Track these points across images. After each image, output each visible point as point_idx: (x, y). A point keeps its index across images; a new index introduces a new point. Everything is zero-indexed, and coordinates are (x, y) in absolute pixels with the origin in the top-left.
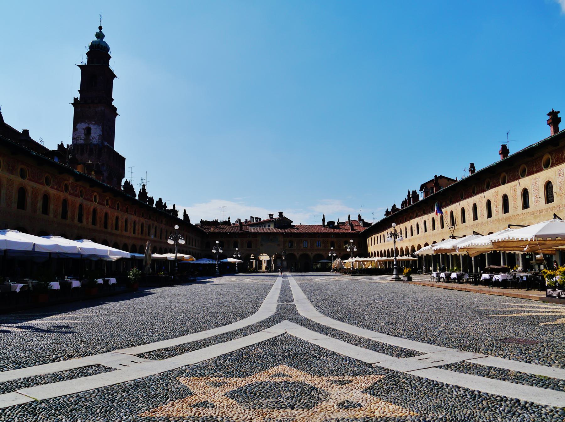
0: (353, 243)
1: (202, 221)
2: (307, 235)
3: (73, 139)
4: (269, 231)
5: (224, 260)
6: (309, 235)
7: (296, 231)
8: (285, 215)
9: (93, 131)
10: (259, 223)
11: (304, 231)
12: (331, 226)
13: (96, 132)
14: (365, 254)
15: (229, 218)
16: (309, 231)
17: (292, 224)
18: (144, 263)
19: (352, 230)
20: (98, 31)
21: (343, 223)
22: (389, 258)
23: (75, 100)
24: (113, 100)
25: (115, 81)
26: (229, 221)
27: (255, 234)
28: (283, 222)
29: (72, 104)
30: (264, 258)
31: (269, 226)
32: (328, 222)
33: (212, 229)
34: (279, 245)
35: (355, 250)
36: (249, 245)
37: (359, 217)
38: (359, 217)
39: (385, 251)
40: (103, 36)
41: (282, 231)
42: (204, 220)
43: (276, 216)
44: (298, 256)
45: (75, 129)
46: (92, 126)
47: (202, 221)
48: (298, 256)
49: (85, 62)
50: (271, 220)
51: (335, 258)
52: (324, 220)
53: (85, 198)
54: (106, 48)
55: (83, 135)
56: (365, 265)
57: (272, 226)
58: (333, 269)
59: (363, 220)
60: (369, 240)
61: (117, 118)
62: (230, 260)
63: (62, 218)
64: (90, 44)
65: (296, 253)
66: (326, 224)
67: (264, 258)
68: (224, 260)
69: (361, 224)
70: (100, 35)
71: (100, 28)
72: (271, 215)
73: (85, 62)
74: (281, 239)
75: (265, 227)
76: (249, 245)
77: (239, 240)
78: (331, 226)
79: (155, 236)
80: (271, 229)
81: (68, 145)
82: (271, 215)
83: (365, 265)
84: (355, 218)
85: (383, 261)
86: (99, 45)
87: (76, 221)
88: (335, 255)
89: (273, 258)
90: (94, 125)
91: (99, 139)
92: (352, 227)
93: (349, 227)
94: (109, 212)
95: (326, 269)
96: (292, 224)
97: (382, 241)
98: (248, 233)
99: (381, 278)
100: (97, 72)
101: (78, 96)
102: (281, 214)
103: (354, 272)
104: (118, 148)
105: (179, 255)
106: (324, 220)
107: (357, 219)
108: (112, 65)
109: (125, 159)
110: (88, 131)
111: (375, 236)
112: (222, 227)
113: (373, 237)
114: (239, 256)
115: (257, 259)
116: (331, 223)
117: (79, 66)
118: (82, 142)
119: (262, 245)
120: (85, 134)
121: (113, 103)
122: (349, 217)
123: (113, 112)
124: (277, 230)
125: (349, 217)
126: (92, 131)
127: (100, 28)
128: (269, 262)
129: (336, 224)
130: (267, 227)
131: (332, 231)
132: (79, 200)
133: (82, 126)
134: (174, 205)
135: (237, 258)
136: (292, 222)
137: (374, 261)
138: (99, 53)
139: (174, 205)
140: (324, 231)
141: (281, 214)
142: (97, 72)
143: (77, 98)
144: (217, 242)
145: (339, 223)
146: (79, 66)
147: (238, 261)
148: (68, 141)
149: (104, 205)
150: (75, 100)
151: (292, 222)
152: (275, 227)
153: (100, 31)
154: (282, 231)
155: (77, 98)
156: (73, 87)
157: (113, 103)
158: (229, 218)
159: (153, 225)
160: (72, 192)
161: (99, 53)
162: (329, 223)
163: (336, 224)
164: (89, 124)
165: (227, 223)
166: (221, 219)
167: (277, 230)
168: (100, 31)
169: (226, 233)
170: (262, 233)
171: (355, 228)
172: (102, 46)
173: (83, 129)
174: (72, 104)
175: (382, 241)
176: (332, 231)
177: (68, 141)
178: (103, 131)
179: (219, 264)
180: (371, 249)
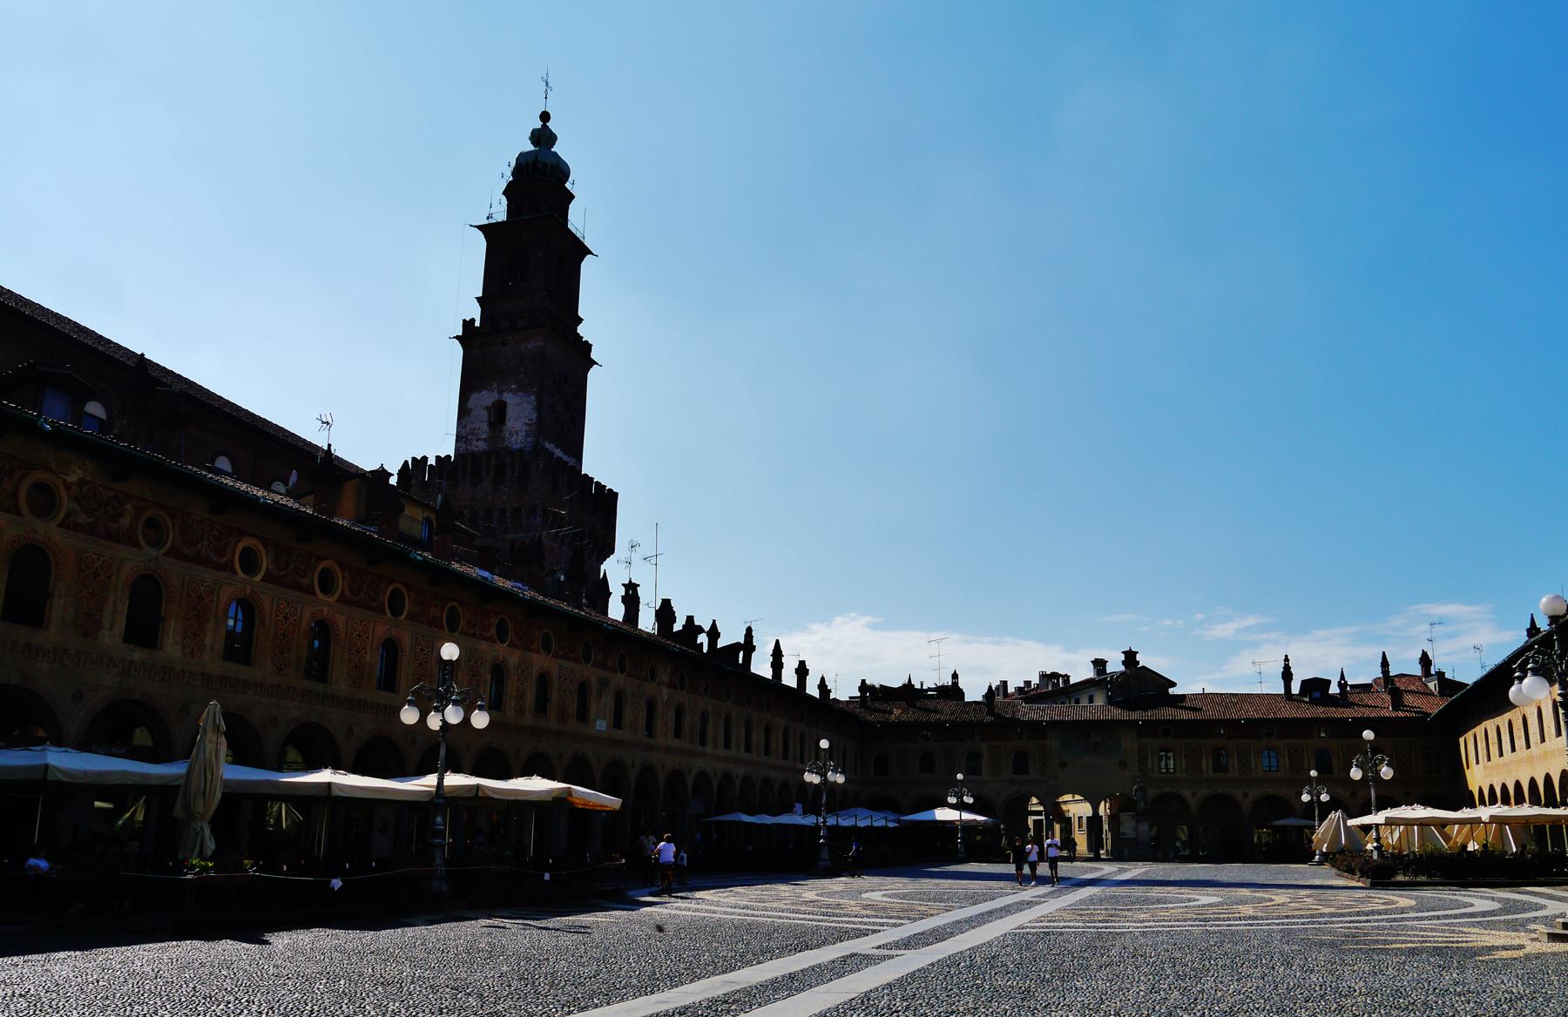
0: (1376, 747)
1: (864, 687)
2: (1228, 728)
3: (459, 438)
4: (1087, 716)
5: (922, 816)
6: (1232, 726)
7: (1184, 715)
8: (1143, 660)
9: (511, 412)
10: (1053, 687)
11: (1210, 713)
12: (1317, 695)
13: (520, 414)
14: (1462, 798)
15: (955, 676)
16: (1233, 715)
17: (1172, 691)
18: (178, 812)
19: (1396, 708)
20: (539, 124)
21: (1365, 688)
22: (1551, 811)
23: (468, 324)
24: (580, 320)
25: (587, 265)
26: (955, 684)
27: (1035, 727)
28: (1137, 685)
29: (457, 337)
30: (1077, 808)
31: (1091, 700)
32: (1305, 683)
33: (896, 712)
34: (1123, 764)
35: (1386, 772)
36: (1021, 766)
37: (1425, 661)
38: (1425, 661)
39: (1533, 782)
40: (552, 138)
41: (1134, 716)
42: (874, 680)
43: (1115, 665)
44: (1193, 803)
45: (464, 411)
46: (509, 398)
47: (864, 687)
48: (1193, 803)
49: (500, 215)
50: (1101, 677)
51: (1325, 810)
52: (1287, 675)
53: (173, 553)
54: (561, 171)
55: (485, 427)
56: (1447, 838)
57: (1100, 701)
58: (1323, 854)
59: (1440, 675)
60: (1468, 743)
61: (593, 374)
62: (943, 814)
63: (130, 637)
64: (513, 164)
65: (1187, 793)
66: (1295, 689)
67: (1077, 808)
68: (922, 816)
69: (1432, 685)
70: (543, 137)
71: (545, 117)
72: (1099, 664)
73: (500, 215)
74: (1129, 742)
75: (1077, 702)
76: (1021, 766)
77: (984, 748)
78: (1317, 695)
79: (617, 723)
80: (1098, 707)
81: (438, 458)
82: (1099, 664)
83: (1447, 838)
84: (1405, 664)
85: (1525, 821)
86: (536, 162)
87: (112, 635)
88: (1324, 797)
89: (1103, 810)
90: (515, 392)
91: (527, 435)
92: (1397, 696)
93: (1388, 698)
94: (340, 620)
95: (1295, 849)
96: (1172, 691)
97: (1520, 742)
98: (1015, 722)
99: (1510, 907)
100: (533, 248)
101: (475, 313)
102: (1130, 656)
103: (1384, 871)
104: (597, 463)
105: (453, 780)
106: (1287, 675)
107: (1417, 670)
108: (579, 219)
109: (613, 496)
110: (499, 412)
111: (1490, 725)
112: (931, 705)
113: (1479, 730)
114: (969, 800)
115: (1056, 814)
116: (1316, 687)
117: (480, 228)
118: (482, 446)
119: (1063, 765)
120: (491, 424)
121: (581, 330)
122: (1385, 664)
123: (582, 356)
124: (1117, 713)
125: (1385, 664)
126: (510, 413)
127: (545, 117)
128: (1094, 822)
129: (1334, 689)
130: (1084, 702)
131: (1320, 712)
132: (131, 561)
133: (486, 398)
134: (749, 630)
135: (961, 806)
136: (1173, 684)
137: (1478, 821)
138: (539, 183)
139: (749, 630)
140: (1289, 712)
141: (1130, 656)
142: (533, 248)
143: (473, 320)
144: (824, 744)
145: (1342, 685)
146: (480, 228)
147: (967, 816)
148: (445, 445)
149: (309, 590)
150: (468, 324)
151: (1173, 684)
152: (1111, 701)
153: (545, 126)
154: (1134, 716)
155: (473, 320)
156: (459, 287)
157: (581, 330)
158: (955, 676)
159: (604, 683)
160: (83, 519)
161: (539, 183)
162: (1308, 685)
163: (1334, 689)
164: (500, 392)
165: (952, 692)
166: (928, 679)
167: (1117, 713)
168: (545, 126)
169: (939, 725)
170: (1061, 722)
171: (1409, 699)
172: (545, 164)
173: (487, 408)
174: (457, 337)
175: (1520, 742)
176: (1320, 712)
177: (439, 441)
178: (539, 409)
179: (829, 828)
180: (1478, 777)
